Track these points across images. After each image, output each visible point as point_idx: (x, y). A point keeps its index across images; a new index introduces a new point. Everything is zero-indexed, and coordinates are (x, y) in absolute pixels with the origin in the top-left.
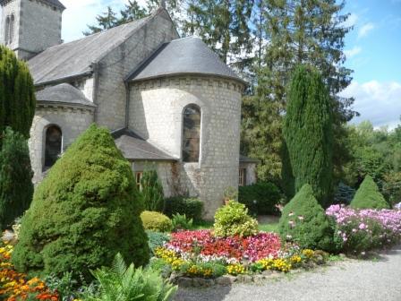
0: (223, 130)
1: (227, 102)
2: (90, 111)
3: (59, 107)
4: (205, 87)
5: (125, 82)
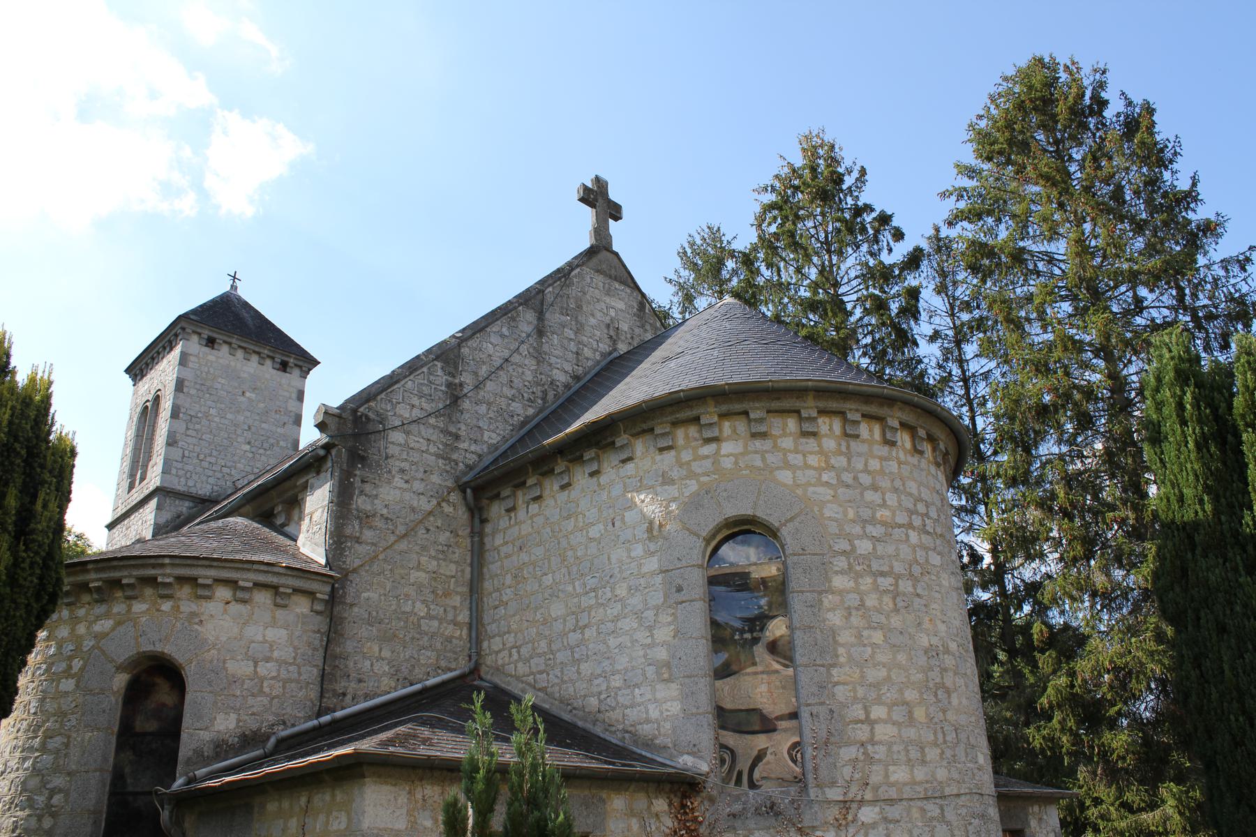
0: (896, 621)
1: (891, 499)
2: (311, 594)
3: (181, 580)
4: (787, 443)
5: (462, 488)
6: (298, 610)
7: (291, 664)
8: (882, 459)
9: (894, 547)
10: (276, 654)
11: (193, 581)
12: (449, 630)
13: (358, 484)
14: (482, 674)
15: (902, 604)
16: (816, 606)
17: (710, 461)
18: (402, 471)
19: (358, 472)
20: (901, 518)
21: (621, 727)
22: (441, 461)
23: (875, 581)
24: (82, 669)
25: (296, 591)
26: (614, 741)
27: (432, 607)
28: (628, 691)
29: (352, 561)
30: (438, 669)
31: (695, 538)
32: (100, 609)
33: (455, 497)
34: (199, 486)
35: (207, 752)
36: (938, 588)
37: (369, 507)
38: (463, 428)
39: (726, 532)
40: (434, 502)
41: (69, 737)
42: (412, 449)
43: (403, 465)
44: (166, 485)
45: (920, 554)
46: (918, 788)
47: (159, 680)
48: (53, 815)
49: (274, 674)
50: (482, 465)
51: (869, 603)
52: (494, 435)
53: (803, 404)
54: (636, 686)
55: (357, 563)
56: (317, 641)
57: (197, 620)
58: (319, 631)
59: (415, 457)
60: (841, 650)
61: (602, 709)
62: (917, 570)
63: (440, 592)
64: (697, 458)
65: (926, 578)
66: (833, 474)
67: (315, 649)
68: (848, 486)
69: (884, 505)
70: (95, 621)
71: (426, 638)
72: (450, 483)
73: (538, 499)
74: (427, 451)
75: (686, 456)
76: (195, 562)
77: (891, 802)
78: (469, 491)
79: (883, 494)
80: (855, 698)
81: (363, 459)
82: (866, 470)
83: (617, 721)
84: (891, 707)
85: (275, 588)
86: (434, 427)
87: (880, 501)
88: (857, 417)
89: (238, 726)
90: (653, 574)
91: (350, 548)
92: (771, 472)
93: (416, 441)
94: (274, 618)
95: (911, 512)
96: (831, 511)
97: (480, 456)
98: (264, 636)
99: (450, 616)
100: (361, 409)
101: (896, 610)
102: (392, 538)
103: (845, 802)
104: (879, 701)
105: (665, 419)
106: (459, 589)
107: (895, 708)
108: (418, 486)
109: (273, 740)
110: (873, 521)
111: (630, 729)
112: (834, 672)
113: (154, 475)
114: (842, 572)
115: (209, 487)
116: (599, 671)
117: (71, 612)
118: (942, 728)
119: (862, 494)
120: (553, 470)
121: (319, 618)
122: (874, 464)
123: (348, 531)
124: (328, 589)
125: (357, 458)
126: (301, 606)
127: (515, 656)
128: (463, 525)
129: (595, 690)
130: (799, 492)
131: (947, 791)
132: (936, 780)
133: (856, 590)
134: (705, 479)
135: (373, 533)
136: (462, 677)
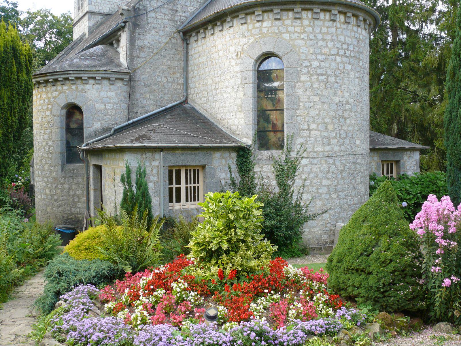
0: (325, 93)
1: (330, 44)
2: (122, 80)
4: (288, 22)
5: (179, 32)
6: (118, 85)
7: (117, 104)
8: (328, 27)
9: (328, 64)
10: (112, 101)
11: (81, 78)
12: (176, 86)
13: (137, 35)
14: (189, 102)
15: (329, 86)
16: (293, 87)
17: (259, 29)
18: (155, 28)
19: (137, 31)
20: (334, 52)
21: (227, 126)
22: (170, 22)
23: (318, 77)
24: (52, 108)
25: (116, 79)
26: (225, 131)
27: (169, 79)
28: (229, 114)
29: (137, 65)
30: (172, 101)
31: (252, 60)
32: (54, 88)
33: (176, 36)
34: (104, 9)
35: (93, 134)
36: (347, 79)
37: (142, 44)
38: (179, 7)
39: (264, 57)
40: (168, 38)
41: (51, 130)
42: (158, 18)
43: (155, 25)
44: (91, 10)
45: (341, 66)
46: (326, 153)
47: (76, 111)
48: (51, 153)
49: (112, 108)
50: (188, 21)
51: (315, 86)
52: (192, 8)
53: (295, 7)
54: (231, 112)
55: (139, 65)
56: (126, 94)
57: (84, 91)
58: (126, 92)
59: (160, 21)
60: (301, 104)
61: (222, 119)
62: (338, 72)
63: (171, 73)
64: (254, 28)
65: (342, 75)
66: (306, 35)
67: (125, 98)
68: (311, 40)
69: (327, 46)
70: (53, 92)
71: (167, 90)
72: (174, 30)
73: (204, 38)
74: (165, 19)
75: (250, 27)
76: (81, 72)
77: (314, 158)
78: (181, 33)
79: (327, 42)
80: (305, 121)
81: (138, 26)
82: (321, 33)
83: (225, 124)
84: (318, 125)
85: (109, 79)
86: (167, 8)
87: (325, 45)
88: (318, 11)
89: (101, 126)
90: (237, 72)
91: (136, 60)
92: (281, 34)
93: (160, 15)
94: (110, 89)
95: (339, 49)
96: (303, 50)
97: (186, 17)
98: (107, 95)
99: (176, 81)
100: (137, 6)
101: (326, 88)
102: (152, 54)
103: (297, 157)
104: (314, 122)
105: (242, 12)
106: (179, 71)
107: (320, 125)
108: (162, 33)
109: (113, 130)
110: (321, 54)
111: (229, 127)
112: (298, 112)
113: (86, 5)
114: (305, 74)
115: (108, 9)
116: (221, 106)
117: (46, 89)
118: (339, 132)
119: (317, 43)
120: (208, 28)
121: (126, 87)
122: (325, 30)
123: (135, 54)
124: (128, 77)
125: (136, 25)
126: (119, 84)
127: (198, 97)
128: (180, 46)
129: (220, 112)
130: (291, 42)
131: (338, 154)
132: (334, 150)
133: (310, 81)
134: (257, 37)
135: (144, 53)
136: (181, 103)
